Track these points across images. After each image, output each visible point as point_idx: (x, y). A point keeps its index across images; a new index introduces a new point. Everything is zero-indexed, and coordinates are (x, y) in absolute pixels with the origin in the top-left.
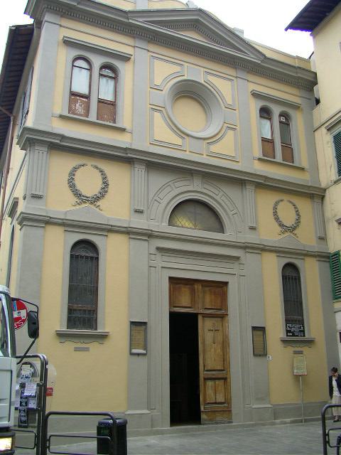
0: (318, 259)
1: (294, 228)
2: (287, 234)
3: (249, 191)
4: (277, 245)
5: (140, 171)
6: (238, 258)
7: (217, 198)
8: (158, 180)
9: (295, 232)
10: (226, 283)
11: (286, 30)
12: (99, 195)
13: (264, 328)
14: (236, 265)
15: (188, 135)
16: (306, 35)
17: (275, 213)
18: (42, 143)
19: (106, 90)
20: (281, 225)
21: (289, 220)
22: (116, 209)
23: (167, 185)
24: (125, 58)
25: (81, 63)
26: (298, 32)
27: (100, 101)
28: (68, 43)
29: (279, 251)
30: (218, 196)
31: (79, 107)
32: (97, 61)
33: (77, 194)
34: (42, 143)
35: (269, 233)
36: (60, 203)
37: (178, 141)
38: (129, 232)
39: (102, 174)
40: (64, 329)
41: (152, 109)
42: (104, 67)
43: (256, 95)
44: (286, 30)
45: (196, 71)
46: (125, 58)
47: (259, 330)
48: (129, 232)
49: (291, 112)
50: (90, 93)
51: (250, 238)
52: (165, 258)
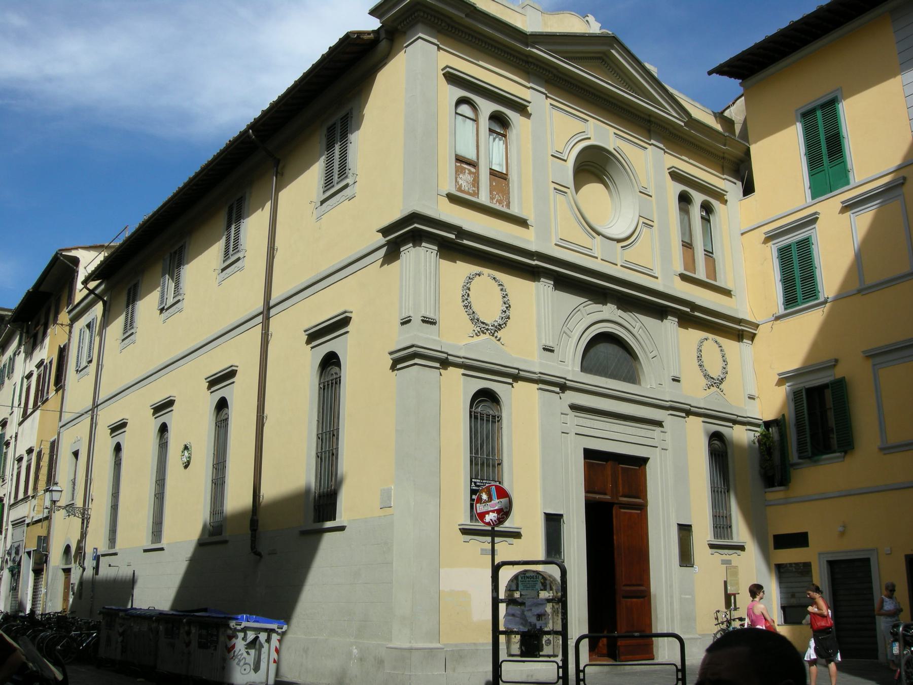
0: (463, 371)
1: (499, 327)
2: (483, 337)
3: (671, 323)
4: (462, 354)
5: (545, 287)
6: (659, 424)
7: (634, 331)
8: (571, 300)
9: (499, 334)
10: (645, 460)
11: (710, 73)
12: (722, 376)
13: (690, 526)
14: (659, 429)
15: (599, 234)
16: (734, 84)
17: (466, 297)
18: (549, 274)
19: (495, 154)
20: (475, 320)
21: (490, 313)
22: (519, 348)
23: (576, 309)
24: (521, 108)
25: (465, 109)
26: (725, 78)
27: (493, 173)
28: (453, 78)
29: (470, 367)
30: (638, 328)
31: (465, 180)
32: (487, 107)
33: (475, 320)
34: (549, 274)
35: (694, 392)
36: (456, 337)
37: (581, 237)
38: (543, 381)
39: (502, 290)
40: (469, 523)
41: (555, 189)
42: (461, 101)
43: (676, 176)
44: (710, 73)
45: (603, 133)
46: (521, 108)
47: (685, 530)
48: (543, 381)
49: (715, 203)
50: (478, 159)
51: (668, 393)
52: (582, 421)
